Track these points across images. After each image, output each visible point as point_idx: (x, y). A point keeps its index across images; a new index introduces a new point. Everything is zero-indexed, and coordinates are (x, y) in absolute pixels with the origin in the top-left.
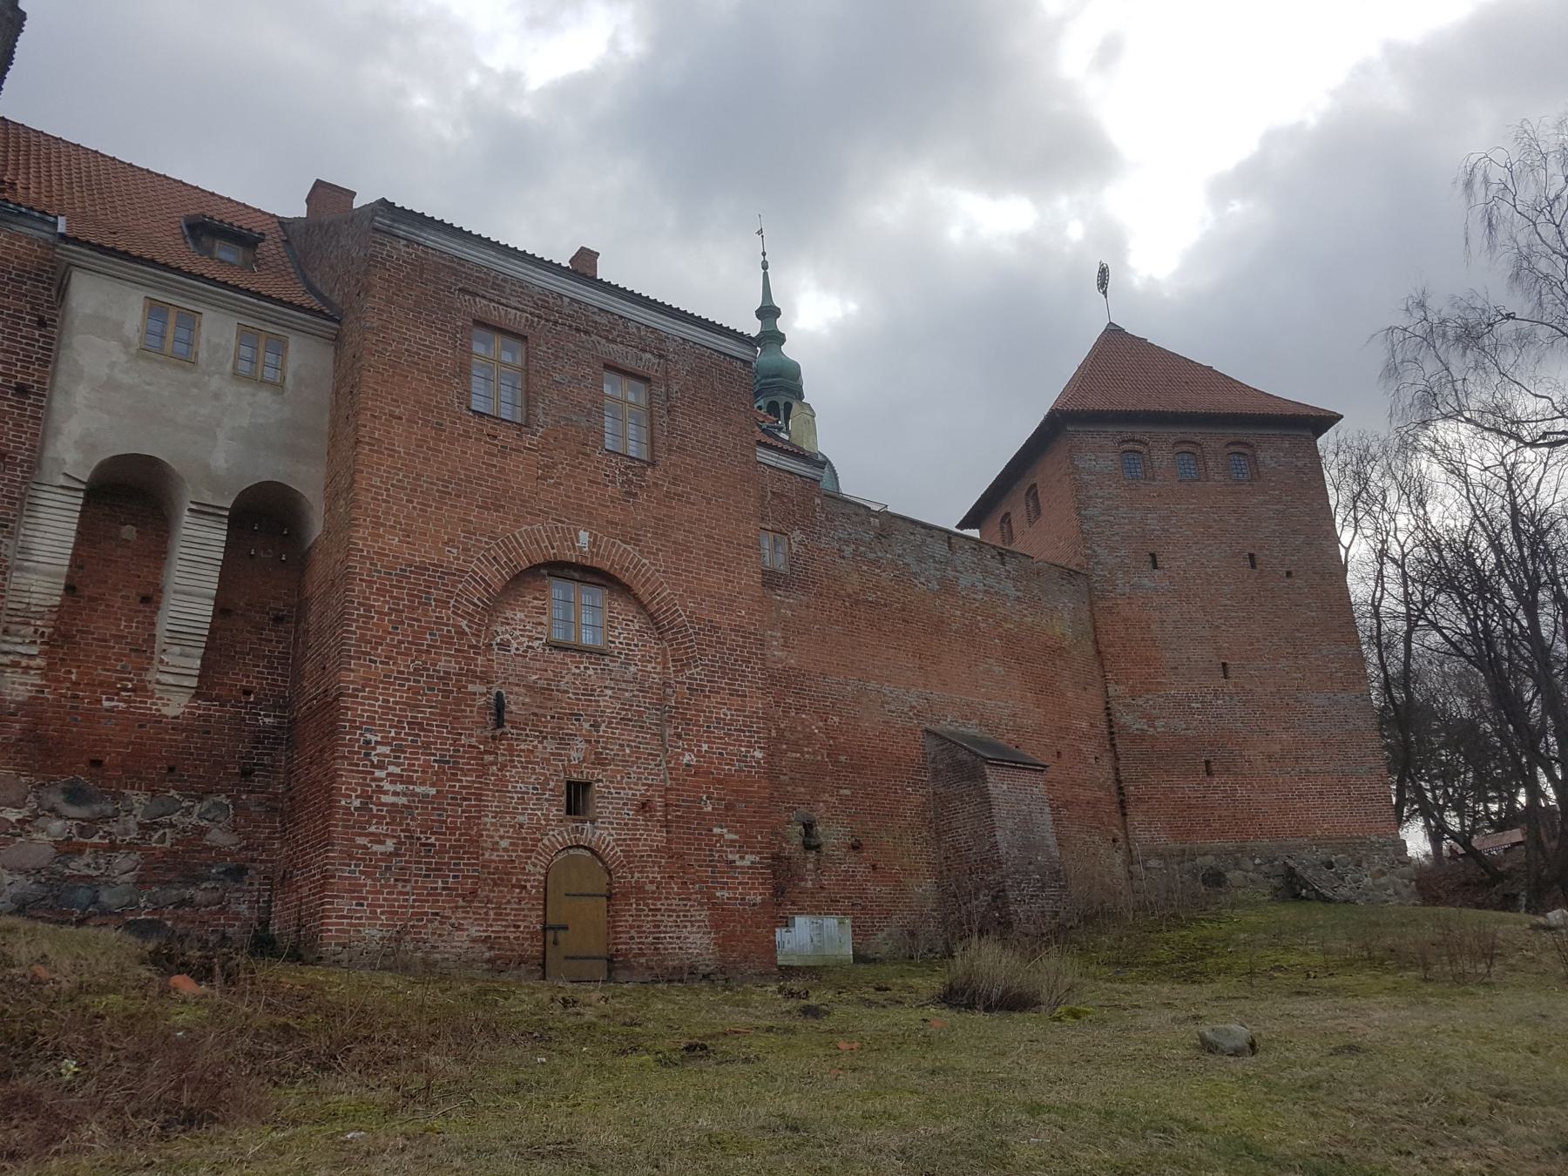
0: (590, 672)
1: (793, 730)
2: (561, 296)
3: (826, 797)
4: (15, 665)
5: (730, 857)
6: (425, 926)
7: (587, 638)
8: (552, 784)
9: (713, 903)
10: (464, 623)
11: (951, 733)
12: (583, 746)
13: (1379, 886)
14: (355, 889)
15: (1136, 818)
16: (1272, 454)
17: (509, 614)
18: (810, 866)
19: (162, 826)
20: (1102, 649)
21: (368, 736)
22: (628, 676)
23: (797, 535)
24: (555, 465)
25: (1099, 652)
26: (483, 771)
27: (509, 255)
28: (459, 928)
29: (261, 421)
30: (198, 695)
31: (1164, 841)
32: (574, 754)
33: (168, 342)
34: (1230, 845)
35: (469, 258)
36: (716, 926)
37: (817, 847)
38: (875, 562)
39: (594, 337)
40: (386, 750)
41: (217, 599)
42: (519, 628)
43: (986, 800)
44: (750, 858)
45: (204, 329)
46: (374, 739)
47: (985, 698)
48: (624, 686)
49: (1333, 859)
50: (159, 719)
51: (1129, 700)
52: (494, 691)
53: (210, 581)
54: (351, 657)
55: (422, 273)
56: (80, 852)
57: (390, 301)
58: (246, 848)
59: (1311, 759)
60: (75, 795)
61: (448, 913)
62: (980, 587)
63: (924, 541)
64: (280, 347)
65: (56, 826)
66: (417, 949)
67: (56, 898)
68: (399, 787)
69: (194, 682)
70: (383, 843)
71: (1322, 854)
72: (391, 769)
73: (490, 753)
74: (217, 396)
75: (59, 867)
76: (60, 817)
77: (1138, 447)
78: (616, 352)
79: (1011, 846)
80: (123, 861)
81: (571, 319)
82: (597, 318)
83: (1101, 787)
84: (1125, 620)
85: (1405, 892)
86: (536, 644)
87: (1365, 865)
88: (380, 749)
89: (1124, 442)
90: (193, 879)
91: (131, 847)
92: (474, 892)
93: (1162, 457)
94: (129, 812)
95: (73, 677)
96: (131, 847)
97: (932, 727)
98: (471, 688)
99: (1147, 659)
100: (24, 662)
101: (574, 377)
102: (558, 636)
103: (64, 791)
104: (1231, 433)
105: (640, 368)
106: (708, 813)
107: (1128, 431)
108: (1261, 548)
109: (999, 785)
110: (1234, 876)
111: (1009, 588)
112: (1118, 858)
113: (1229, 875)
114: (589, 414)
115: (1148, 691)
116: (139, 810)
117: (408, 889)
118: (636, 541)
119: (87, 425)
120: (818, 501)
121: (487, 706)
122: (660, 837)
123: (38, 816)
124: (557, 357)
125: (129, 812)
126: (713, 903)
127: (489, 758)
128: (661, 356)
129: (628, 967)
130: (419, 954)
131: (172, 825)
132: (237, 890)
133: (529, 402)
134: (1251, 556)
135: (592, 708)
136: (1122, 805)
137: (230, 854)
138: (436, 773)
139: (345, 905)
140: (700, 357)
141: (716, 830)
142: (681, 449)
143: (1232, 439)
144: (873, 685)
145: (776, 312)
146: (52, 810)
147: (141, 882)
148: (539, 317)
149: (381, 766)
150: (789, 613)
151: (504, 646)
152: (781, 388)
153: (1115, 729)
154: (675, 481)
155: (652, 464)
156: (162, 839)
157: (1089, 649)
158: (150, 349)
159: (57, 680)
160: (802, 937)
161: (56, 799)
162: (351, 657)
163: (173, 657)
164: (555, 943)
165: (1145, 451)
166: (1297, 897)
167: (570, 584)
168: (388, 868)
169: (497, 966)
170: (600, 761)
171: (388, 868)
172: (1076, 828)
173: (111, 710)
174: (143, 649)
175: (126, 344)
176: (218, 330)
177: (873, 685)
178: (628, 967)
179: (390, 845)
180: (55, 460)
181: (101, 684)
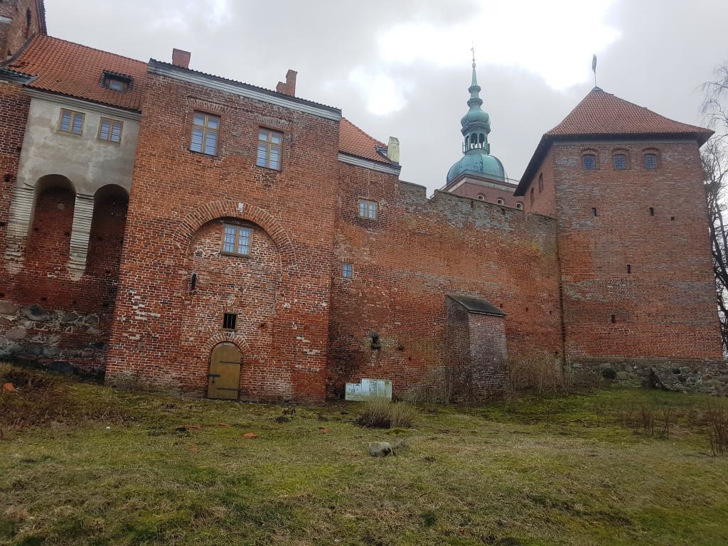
0: (241, 266)
2: (239, 96)
4: (12, 260)
5: (304, 350)
9: (293, 370)
10: (178, 245)
11: (460, 298)
13: (707, 384)
14: (121, 354)
15: (570, 342)
16: (670, 155)
17: (203, 240)
18: (374, 357)
19: (69, 325)
20: (561, 257)
22: (260, 268)
23: (383, 202)
25: (559, 259)
26: (184, 307)
29: (109, 158)
30: (86, 272)
31: (585, 354)
32: (229, 302)
33: (71, 128)
34: (621, 358)
35: (194, 82)
36: (294, 380)
37: (379, 348)
38: (427, 215)
39: (255, 114)
40: (139, 297)
42: (206, 246)
43: (468, 330)
44: (314, 352)
45: (86, 120)
46: (133, 293)
47: (486, 279)
48: (257, 272)
49: (680, 368)
50: (70, 282)
53: (87, 226)
54: (125, 258)
56: (37, 334)
57: (153, 104)
58: (104, 335)
59: (674, 316)
60: (35, 311)
62: (488, 225)
63: (456, 204)
64: (121, 125)
65: (28, 323)
68: (143, 313)
69: (84, 268)
70: (135, 336)
71: (674, 366)
72: (141, 305)
74: (90, 149)
75: (28, 339)
77: (593, 153)
78: (267, 120)
79: (478, 352)
81: (237, 110)
82: (257, 105)
83: (551, 326)
84: (575, 243)
86: (214, 253)
88: (136, 297)
90: (81, 347)
91: (57, 332)
92: (175, 358)
95: (37, 265)
96: (57, 332)
97: (451, 294)
98: (180, 272)
99: (585, 262)
100: (16, 259)
101: (243, 133)
103: (31, 309)
104: (647, 144)
105: (279, 127)
106: (295, 330)
108: (658, 205)
109: (475, 323)
110: (621, 374)
111: (507, 227)
112: (558, 362)
113: (618, 374)
115: (584, 279)
116: (60, 319)
117: (145, 355)
119: (35, 163)
121: (188, 280)
122: (269, 339)
123: (20, 319)
124: (235, 124)
126: (293, 370)
127: (187, 302)
128: (290, 121)
130: (148, 382)
131: (74, 325)
132: (100, 352)
133: (219, 145)
134: (652, 209)
135: (248, 281)
139: (117, 360)
140: (311, 120)
141: (298, 338)
145: (479, 102)
146: (26, 317)
147: (61, 347)
149: (136, 304)
150: (374, 239)
151: (199, 254)
155: (280, 172)
156: (70, 330)
157: (553, 257)
159: (30, 266)
160: (362, 389)
161: (28, 313)
162: (125, 258)
163: (74, 257)
164: (213, 382)
165: (596, 154)
166: (654, 387)
168: (136, 346)
169: (183, 390)
170: (242, 305)
171: (136, 346)
173: (51, 278)
174: (65, 255)
175: (52, 129)
176: (92, 120)
178: (247, 394)
180: (20, 178)
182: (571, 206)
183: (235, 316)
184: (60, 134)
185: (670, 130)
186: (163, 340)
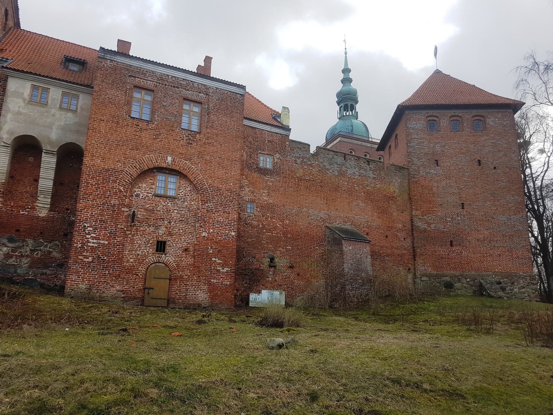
0: (170, 204)
1: (269, 225)
2: (168, 75)
3: (281, 249)
6: (101, 285)
7: (171, 193)
8: (151, 241)
9: (210, 284)
10: (122, 188)
12: (165, 229)
13: (521, 293)
14: (77, 272)
15: (419, 261)
17: (140, 185)
19: (37, 250)
20: (412, 197)
21: (85, 224)
22: (184, 206)
23: (277, 156)
24: (160, 134)
25: (410, 198)
26: (126, 236)
27: (150, 63)
28: (113, 286)
30: (50, 211)
32: (160, 232)
33: (38, 99)
34: (458, 273)
36: (210, 291)
37: (275, 267)
38: (311, 165)
39: (181, 89)
40: (91, 229)
41: (53, 180)
42: (143, 189)
43: (342, 253)
44: (226, 269)
47: (356, 214)
49: (502, 281)
51: (421, 217)
52: (132, 211)
55: (115, 71)
57: (103, 81)
58: (64, 258)
59: (497, 241)
60: (11, 240)
61: (109, 281)
63: (333, 157)
64: (77, 97)
65: (5, 249)
66: (97, 292)
67: (3, 270)
68: (95, 241)
69: (49, 206)
70: (88, 258)
71: (497, 279)
72: (92, 235)
73: (129, 231)
74: (53, 115)
75: (5, 261)
76: (6, 246)
77: (435, 118)
78: (189, 94)
80: (25, 261)
82: (182, 82)
83: (405, 249)
84: (422, 186)
85: (532, 295)
86: (149, 195)
87: (516, 284)
88: (89, 229)
89: (429, 116)
90: (46, 267)
91: (27, 256)
92: (119, 275)
93: (444, 122)
94: (27, 246)
96: (27, 256)
98: (123, 209)
99: (430, 201)
101: (171, 103)
102: (161, 192)
103: (7, 239)
104: (475, 112)
105: (198, 99)
106: (211, 253)
107: (431, 112)
108: (483, 158)
110: (458, 285)
112: (410, 276)
113: (456, 285)
114: (176, 116)
115: (429, 213)
118: (190, 160)
120: (287, 143)
121: (129, 215)
122: (191, 260)
124: (165, 97)
125: (27, 246)
126: (210, 284)
128: (207, 94)
129: (174, 302)
131: (40, 250)
133: (153, 112)
136: (414, 257)
137: (59, 259)
138: (108, 237)
139: (74, 277)
141: (213, 259)
142: (212, 127)
143: (475, 114)
144: (305, 209)
146: (3, 244)
147: (30, 267)
148: (159, 83)
149: (89, 234)
150: (271, 184)
151: (138, 196)
152: (349, 99)
153: (414, 228)
154: (208, 138)
155: (199, 133)
156: (37, 254)
157: (406, 197)
158: (31, 102)
159: (7, 205)
160: (262, 298)
161: (5, 241)
163: (41, 198)
164: (148, 293)
167: (164, 175)
170: (170, 234)
172: (391, 264)
173: (23, 214)
174: (34, 196)
175: (24, 100)
176: (55, 94)
177: (305, 209)
178: (174, 302)
179: (90, 259)
181: (20, 207)
182: (419, 159)
183: (165, 243)
184: (31, 104)
185: (493, 102)
186: (110, 261)
